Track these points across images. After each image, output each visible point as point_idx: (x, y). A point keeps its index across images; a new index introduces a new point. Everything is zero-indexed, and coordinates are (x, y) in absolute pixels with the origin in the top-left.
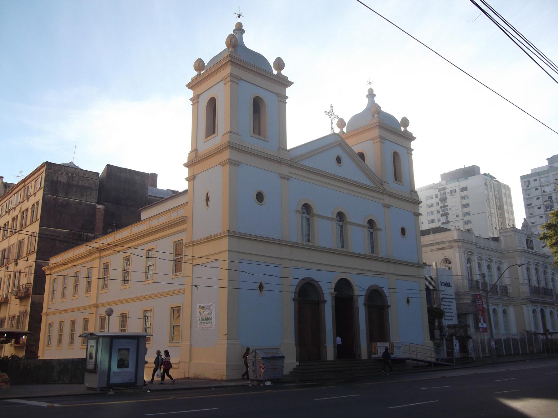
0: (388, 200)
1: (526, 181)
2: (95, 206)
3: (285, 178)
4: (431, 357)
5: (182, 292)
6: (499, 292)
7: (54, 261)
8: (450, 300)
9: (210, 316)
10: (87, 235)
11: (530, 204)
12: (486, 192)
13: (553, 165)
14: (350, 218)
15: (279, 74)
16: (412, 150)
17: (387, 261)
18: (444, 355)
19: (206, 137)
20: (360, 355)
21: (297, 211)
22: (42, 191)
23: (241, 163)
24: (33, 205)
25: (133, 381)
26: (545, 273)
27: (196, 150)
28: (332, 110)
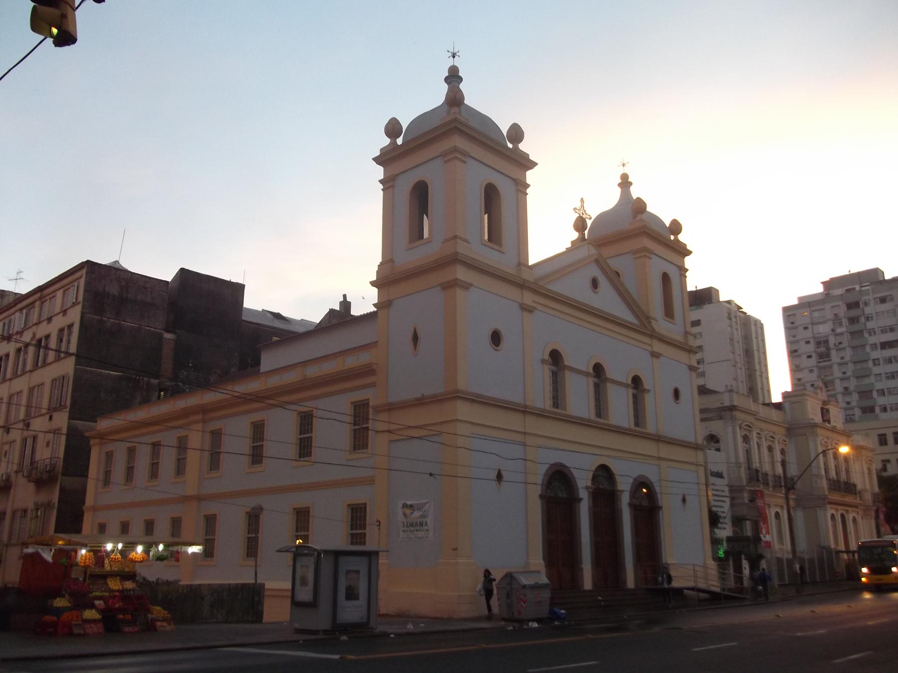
0: (658, 347)
1: (789, 313)
2: (160, 337)
3: (526, 309)
4: (715, 585)
5: (370, 481)
6: (771, 484)
7: (104, 424)
8: (722, 499)
9: (424, 520)
10: (148, 382)
11: (796, 351)
12: (729, 329)
13: (831, 292)
14: (611, 373)
15: (516, 149)
16: (687, 270)
17: (658, 439)
18: (731, 583)
19: (410, 243)
20: (625, 582)
21: (543, 361)
22: (78, 309)
23: (472, 285)
24: (61, 331)
25: (365, 620)
26: (770, 449)
27: (392, 261)
28: (582, 206)
